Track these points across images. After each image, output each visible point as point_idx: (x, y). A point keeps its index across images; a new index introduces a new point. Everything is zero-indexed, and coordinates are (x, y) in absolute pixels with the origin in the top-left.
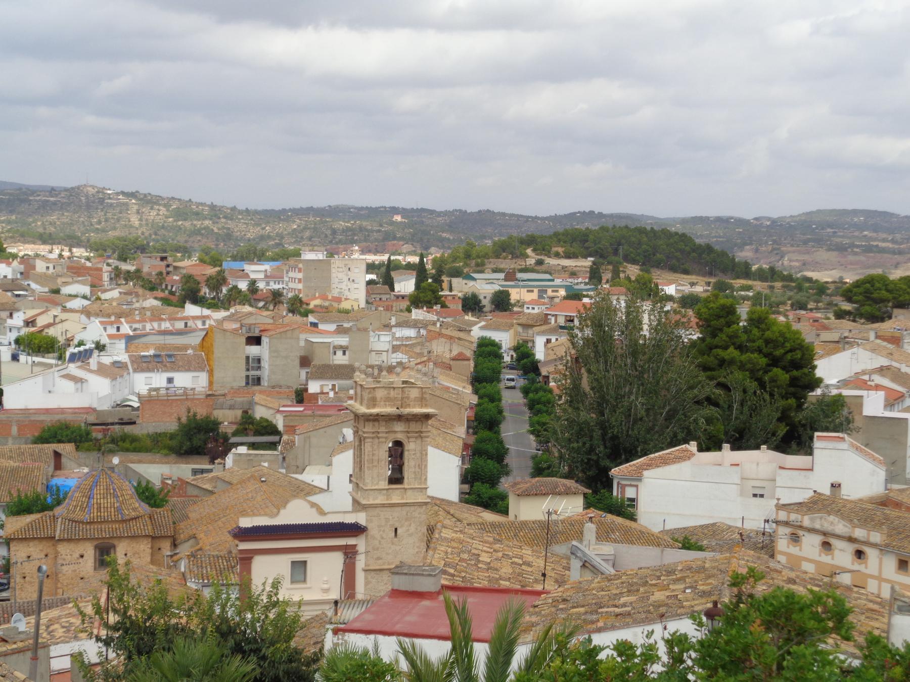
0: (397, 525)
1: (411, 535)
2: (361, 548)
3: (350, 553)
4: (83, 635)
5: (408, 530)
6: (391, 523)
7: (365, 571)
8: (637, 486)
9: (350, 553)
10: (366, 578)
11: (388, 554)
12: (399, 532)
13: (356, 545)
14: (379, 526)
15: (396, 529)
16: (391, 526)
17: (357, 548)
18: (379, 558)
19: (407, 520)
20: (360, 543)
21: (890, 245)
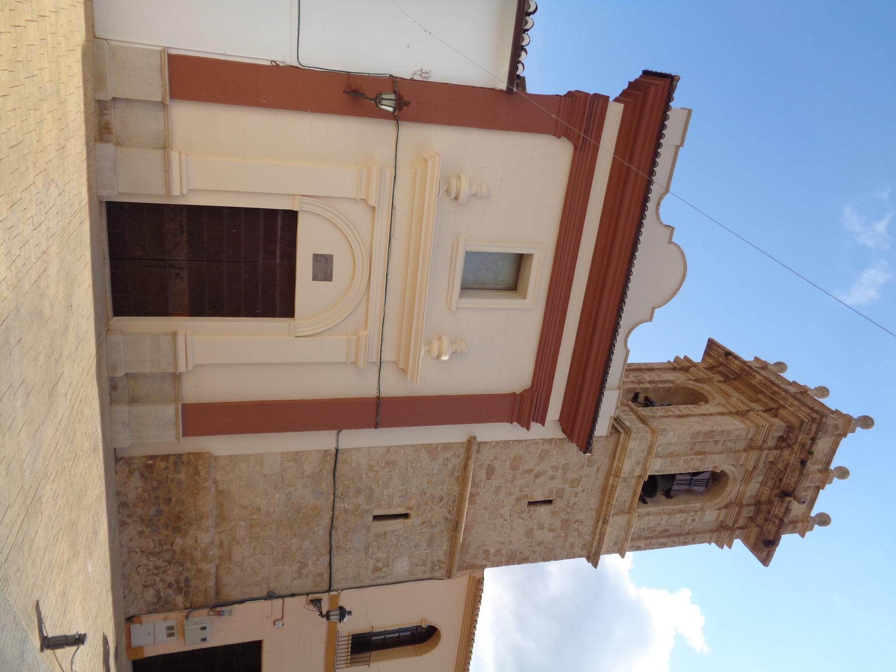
0: (559, 504)
1: (529, 533)
2: (537, 431)
3: (524, 407)
4: (127, 591)
5: (541, 527)
6: (568, 490)
7: (471, 441)
8: (480, 444)
9: (524, 407)
10: (446, 447)
11: (498, 489)
12: (543, 509)
13: (543, 424)
14: (565, 468)
15: (549, 502)
16: (560, 494)
17: (540, 425)
18: (490, 471)
19: (566, 522)
20: (549, 429)
21: (610, 483)
